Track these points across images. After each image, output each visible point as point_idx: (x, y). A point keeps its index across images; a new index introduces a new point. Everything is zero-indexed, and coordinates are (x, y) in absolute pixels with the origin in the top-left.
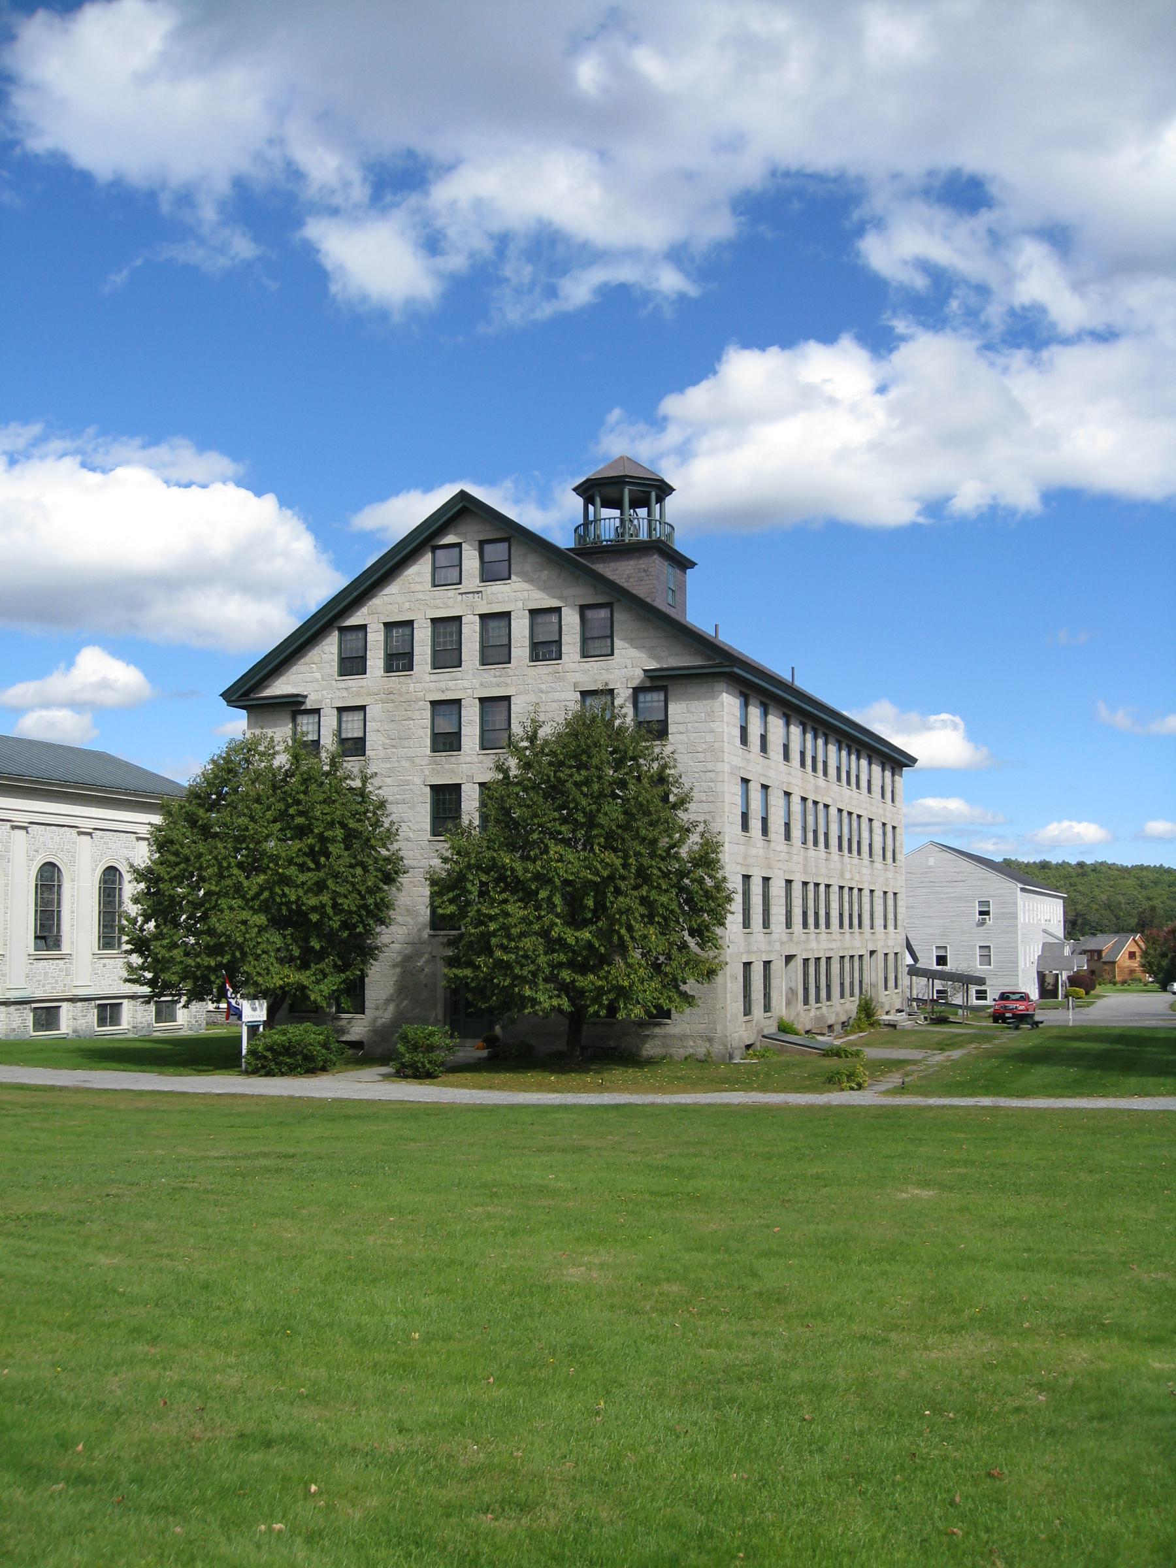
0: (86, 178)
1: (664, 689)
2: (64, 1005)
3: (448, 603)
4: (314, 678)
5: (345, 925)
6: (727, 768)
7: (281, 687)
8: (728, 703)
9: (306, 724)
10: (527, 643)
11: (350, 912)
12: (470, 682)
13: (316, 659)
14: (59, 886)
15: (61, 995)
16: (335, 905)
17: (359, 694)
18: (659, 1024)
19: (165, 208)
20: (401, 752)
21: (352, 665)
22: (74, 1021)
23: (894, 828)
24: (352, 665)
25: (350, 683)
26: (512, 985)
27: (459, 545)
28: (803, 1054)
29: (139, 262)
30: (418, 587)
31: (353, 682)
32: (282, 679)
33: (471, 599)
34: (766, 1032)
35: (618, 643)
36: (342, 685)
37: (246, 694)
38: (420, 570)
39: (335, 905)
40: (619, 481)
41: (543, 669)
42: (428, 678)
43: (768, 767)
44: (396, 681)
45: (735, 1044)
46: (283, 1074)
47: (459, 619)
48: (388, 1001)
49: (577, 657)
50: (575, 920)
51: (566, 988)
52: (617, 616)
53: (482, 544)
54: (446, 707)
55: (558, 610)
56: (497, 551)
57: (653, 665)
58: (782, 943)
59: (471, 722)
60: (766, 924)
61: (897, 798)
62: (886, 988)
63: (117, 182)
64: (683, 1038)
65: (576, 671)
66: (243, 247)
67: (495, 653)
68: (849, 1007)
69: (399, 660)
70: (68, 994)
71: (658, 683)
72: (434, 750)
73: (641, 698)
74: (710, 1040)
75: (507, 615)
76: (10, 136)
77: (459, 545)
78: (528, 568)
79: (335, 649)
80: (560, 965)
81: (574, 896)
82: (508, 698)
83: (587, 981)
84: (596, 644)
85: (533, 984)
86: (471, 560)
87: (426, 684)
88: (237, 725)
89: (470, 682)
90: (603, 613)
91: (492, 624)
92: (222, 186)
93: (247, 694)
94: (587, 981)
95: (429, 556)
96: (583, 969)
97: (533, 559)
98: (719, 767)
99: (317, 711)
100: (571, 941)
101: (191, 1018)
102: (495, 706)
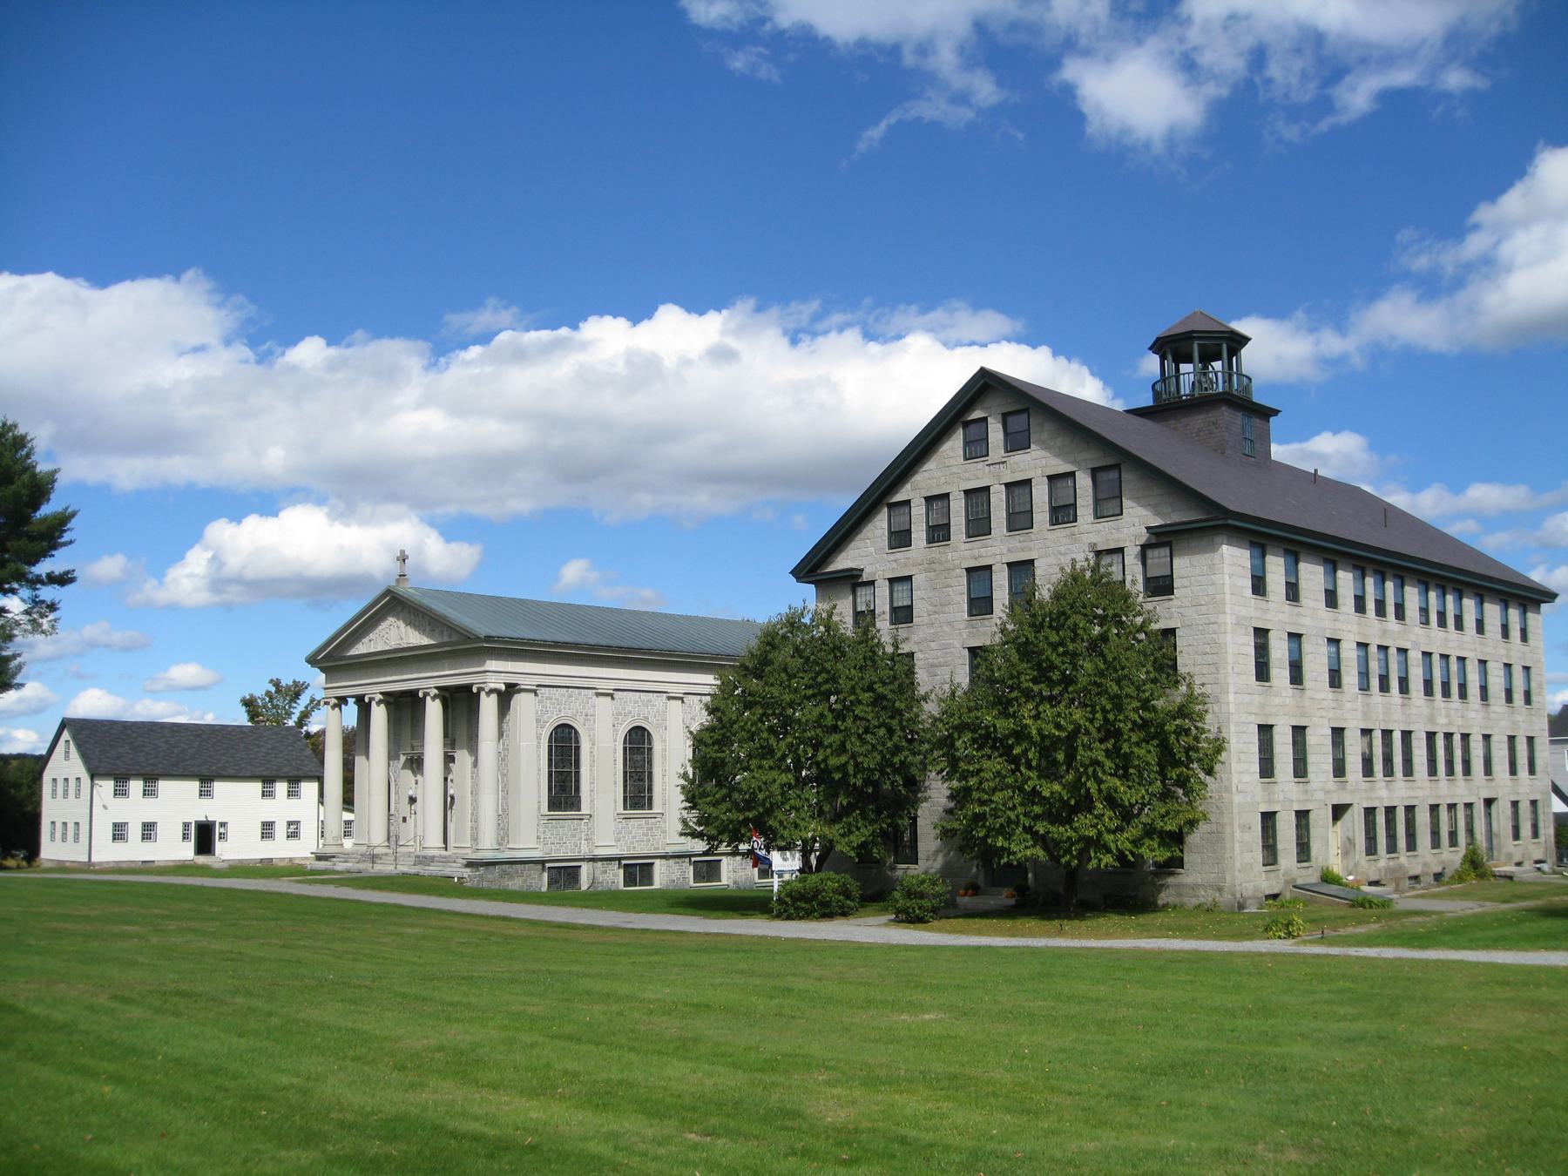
0: (828, 43)
1: (1169, 544)
2: (657, 862)
3: (977, 474)
4: (868, 552)
5: (867, 782)
6: (1229, 619)
7: (842, 562)
8: (1233, 559)
9: (863, 594)
10: (1047, 508)
11: (873, 770)
12: (999, 549)
13: (870, 534)
14: (650, 749)
15: (653, 852)
16: (857, 765)
17: (906, 565)
18: (1172, 874)
19: (909, 59)
20: (942, 617)
21: (901, 538)
22: (663, 875)
23: (1527, 669)
24: (901, 538)
25: (899, 555)
26: (987, 836)
27: (985, 419)
28: (1332, 904)
29: (893, 120)
30: (952, 462)
31: (901, 555)
32: (843, 555)
33: (999, 468)
34: (1300, 882)
35: (1126, 503)
36: (892, 557)
37: (813, 570)
38: (954, 445)
39: (857, 765)
40: (1188, 337)
41: (1062, 532)
42: (963, 546)
43: (1299, 615)
44: (936, 551)
45: (1248, 892)
46: (801, 918)
47: (987, 489)
48: (937, 852)
49: (1091, 519)
50: (1049, 771)
51: (1042, 840)
52: (1124, 476)
53: (1005, 416)
54: (979, 574)
55: (1072, 474)
56: (1018, 422)
57: (1157, 522)
58: (1327, 792)
59: (1000, 586)
60: (1488, 770)
61: (1530, 636)
62: (1516, 836)
63: (862, 43)
64: (1195, 887)
65: (1090, 531)
66: (985, 89)
67: (979, 526)
68: (1452, 857)
69: (939, 533)
70: (661, 851)
71: (1163, 539)
72: (970, 614)
73: (1150, 553)
74: (1220, 889)
75: (1028, 482)
76: (761, 13)
77: (985, 419)
78: (1044, 436)
79: (885, 526)
80: (1036, 818)
81: (1047, 747)
82: (1031, 562)
83: (1060, 832)
84: (1108, 505)
85: (1008, 837)
86: (996, 434)
87: (962, 551)
88: (805, 597)
89: (999, 549)
90: (1113, 475)
91: (1017, 491)
92: (962, 28)
93: (812, 569)
94: (1060, 832)
95: (960, 432)
96: (1055, 819)
97: (1049, 427)
98: (1221, 619)
99: (872, 583)
100: (1046, 793)
101: (734, 872)
102: (1021, 569)
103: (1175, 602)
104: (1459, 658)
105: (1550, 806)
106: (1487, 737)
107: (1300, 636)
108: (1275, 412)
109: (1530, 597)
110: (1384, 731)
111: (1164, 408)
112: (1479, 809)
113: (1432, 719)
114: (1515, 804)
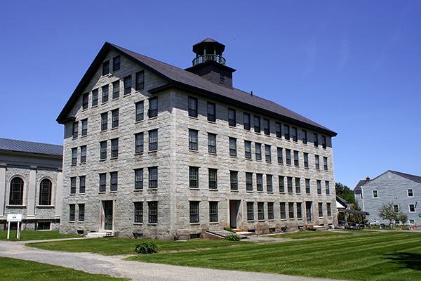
97: (125, 60)
103: (158, 119)
104: (295, 151)
105: (335, 205)
106: (308, 180)
107: (215, 135)
108: (335, 134)
109: (323, 136)
110: (257, 174)
111: (195, 70)
112: (304, 206)
113: (281, 171)
114: (320, 204)
